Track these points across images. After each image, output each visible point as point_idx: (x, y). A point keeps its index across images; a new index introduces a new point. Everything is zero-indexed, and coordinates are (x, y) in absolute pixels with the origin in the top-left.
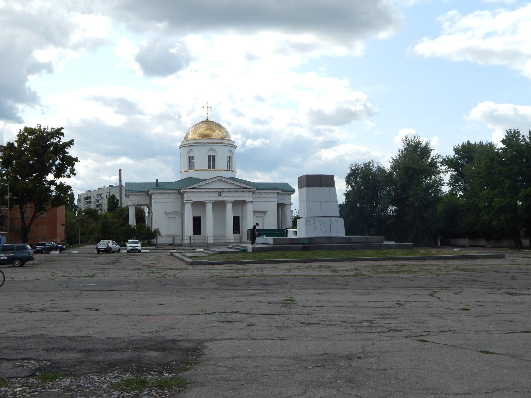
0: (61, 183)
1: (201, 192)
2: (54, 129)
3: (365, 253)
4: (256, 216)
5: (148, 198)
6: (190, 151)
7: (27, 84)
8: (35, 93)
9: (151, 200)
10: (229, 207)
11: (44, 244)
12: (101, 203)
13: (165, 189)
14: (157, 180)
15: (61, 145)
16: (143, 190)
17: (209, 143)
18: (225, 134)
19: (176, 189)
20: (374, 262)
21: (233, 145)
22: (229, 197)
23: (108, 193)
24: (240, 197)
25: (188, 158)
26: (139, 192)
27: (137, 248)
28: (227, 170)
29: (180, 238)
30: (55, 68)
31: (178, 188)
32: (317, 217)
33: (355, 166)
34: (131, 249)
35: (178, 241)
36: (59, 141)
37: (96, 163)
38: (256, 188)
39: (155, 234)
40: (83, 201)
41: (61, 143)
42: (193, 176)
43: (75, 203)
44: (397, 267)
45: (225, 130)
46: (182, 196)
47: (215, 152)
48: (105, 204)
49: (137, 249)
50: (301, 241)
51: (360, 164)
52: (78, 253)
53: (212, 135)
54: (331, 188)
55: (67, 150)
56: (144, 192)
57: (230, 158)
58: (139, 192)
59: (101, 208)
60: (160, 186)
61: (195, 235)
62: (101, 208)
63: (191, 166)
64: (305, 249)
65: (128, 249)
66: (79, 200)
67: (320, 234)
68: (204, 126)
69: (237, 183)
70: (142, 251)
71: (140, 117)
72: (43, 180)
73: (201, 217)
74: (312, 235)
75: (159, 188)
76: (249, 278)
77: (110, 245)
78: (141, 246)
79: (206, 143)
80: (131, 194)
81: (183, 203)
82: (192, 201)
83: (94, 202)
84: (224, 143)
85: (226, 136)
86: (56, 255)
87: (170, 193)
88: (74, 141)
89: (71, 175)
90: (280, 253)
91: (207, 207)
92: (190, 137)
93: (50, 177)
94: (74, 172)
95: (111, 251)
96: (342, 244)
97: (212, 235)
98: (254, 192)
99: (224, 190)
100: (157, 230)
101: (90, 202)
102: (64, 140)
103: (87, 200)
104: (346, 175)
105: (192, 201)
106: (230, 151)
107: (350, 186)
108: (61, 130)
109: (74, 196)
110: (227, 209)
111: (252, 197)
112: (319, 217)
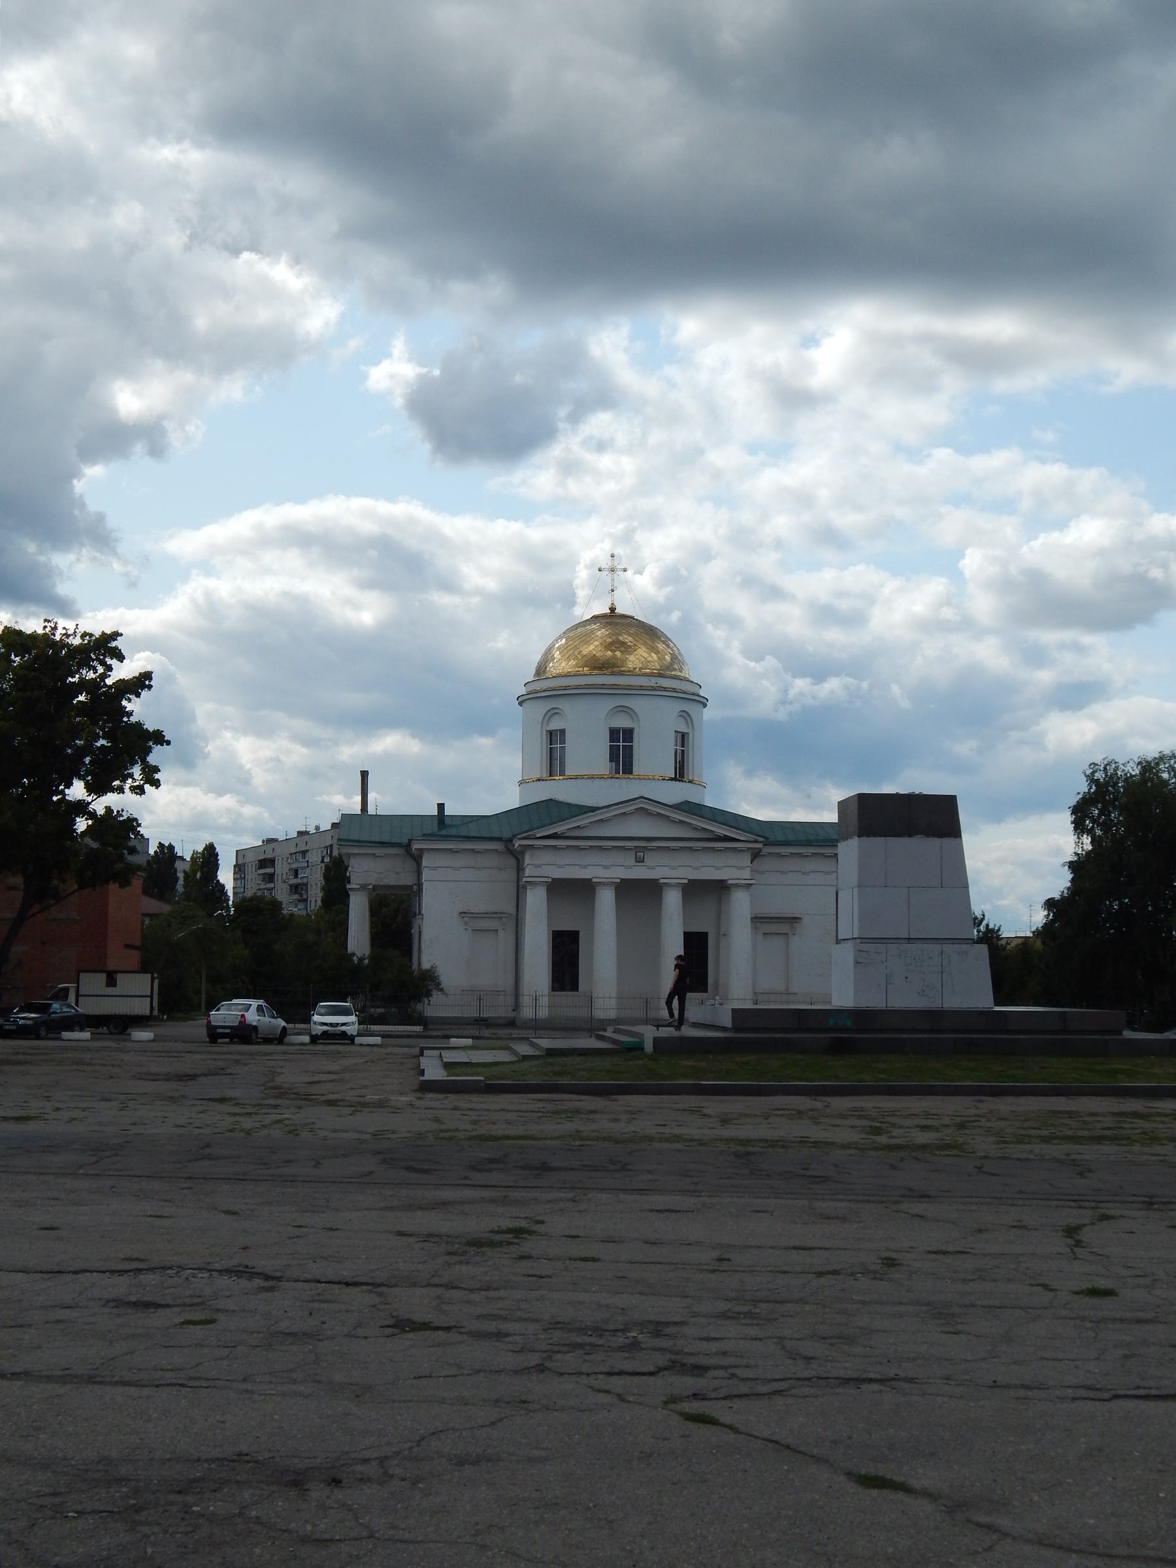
0: (109, 810)
1: (577, 848)
2: (91, 635)
3: (1043, 1068)
4: (764, 934)
5: (411, 865)
6: (552, 712)
7: (79, 486)
8: (101, 518)
9: (419, 873)
10: (673, 900)
11: (44, 1009)
12: (305, 881)
13: (464, 837)
14: (441, 807)
15: (110, 687)
16: (396, 840)
17: (615, 686)
18: (668, 658)
19: (499, 839)
20: (1062, 1099)
21: (693, 694)
22: (672, 868)
23: (327, 847)
24: (710, 868)
25: (544, 737)
26: (383, 844)
27: (344, 1028)
28: (672, 779)
29: (510, 1000)
30: (174, 438)
31: (507, 834)
32: (896, 941)
33: (1105, 768)
34: (325, 1033)
35: (500, 1009)
36: (104, 676)
37: (304, 751)
38: (762, 839)
39: (427, 983)
40: (252, 874)
41: (109, 682)
42: (561, 797)
43: (219, 878)
44: (1119, 1122)
45: (668, 646)
46: (518, 862)
47: (635, 719)
48: (317, 884)
49: (344, 1033)
50: (831, 1022)
51: (1121, 761)
52: (154, 1041)
53: (624, 662)
54: (947, 842)
55: (128, 706)
56: (398, 845)
57: (683, 738)
58: (383, 844)
59: (305, 897)
60: (452, 826)
61: (559, 993)
62: (305, 897)
63: (555, 763)
64: (840, 1047)
65: (313, 1033)
66: (240, 870)
67: (905, 998)
68: (601, 632)
69: (701, 821)
70: (358, 1040)
71: (444, 600)
72: (55, 798)
73: (578, 932)
74: (875, 1001)
75: (443, 832)
76: (540, 1143)
77: (252, 1017)
78: (359, 1024)
79: (603, 686)
80: (355, 851)
81: (521, 883)
82: (550, 880)
83: (284, 876)
84: (665, 689)
85: (670, 667)
86: (81, 1044)
87: (481, 852)
88: (150, 679)
89: (147, 787)
90: (745, 1059)
91: (597, 902)
92: (554, 668)
93: (77, 791)
94: (157, 776)
95: (254, 1035)
96: (971, 1036)
97: (614, 995)
98: (756, 855)
99: (655, 844)
100: (430, 971)
101: (270, 878)
102: (122, 671)
103: (262, 871)
104: (1074, 800)
105: (550, 880)
106: (685, 715)
107: (1087, 840)
108: (115, 640)
109: (217, 855)
110: (663, 907)
111: (749, 869)
112: (902, 941)
